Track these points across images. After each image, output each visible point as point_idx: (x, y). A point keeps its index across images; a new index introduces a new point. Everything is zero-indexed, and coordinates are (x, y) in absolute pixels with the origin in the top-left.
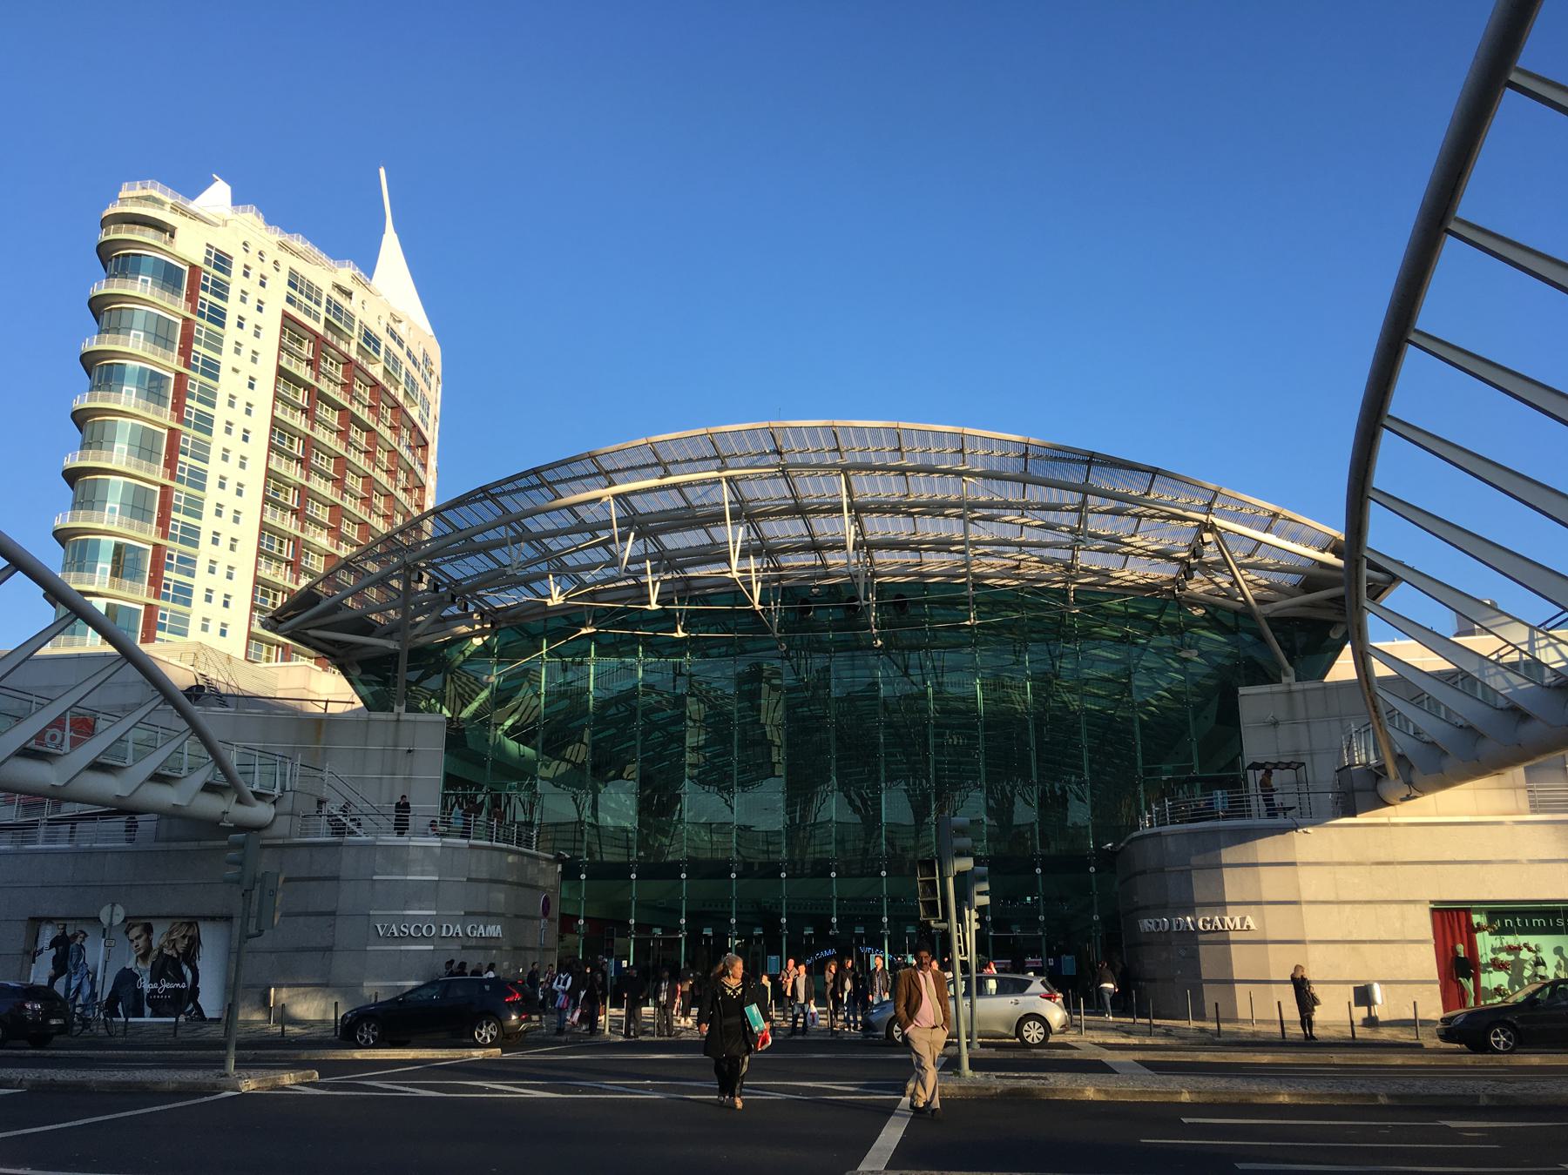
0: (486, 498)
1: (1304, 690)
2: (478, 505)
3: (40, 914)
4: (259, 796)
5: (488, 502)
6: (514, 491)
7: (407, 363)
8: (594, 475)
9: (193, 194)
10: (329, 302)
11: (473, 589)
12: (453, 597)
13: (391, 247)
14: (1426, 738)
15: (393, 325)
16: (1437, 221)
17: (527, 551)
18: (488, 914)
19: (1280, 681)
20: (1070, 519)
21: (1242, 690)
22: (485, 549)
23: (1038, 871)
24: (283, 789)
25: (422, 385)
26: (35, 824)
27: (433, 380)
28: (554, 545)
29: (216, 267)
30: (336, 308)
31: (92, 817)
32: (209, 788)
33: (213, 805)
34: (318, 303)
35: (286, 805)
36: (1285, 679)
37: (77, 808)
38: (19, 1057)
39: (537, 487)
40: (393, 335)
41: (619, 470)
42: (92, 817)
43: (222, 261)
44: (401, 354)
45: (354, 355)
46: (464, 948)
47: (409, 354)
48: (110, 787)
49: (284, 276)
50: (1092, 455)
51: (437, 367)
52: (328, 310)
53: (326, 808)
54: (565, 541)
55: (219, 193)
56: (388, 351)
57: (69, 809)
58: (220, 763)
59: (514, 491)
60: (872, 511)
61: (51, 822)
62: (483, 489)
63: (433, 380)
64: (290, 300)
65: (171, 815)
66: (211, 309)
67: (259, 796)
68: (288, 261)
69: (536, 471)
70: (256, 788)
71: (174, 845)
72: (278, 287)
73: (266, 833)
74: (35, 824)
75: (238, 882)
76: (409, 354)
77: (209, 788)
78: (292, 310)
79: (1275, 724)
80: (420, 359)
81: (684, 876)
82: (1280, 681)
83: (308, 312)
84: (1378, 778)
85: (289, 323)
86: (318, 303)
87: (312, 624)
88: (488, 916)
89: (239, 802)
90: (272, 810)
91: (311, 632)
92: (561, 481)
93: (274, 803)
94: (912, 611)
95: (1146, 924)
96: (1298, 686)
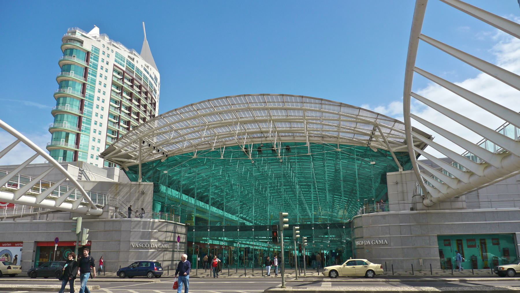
1: (405, 174)
7: (150, 79)
9: (88, 31)
10: (127, 61)
13: (146, 44)
15: (146, 67)
16: (415, 35)
19: (398, 171)
20: (336, 123)
21: (388, 174)
23: (344, 227)
25: (154, 85)
27: (158, 84)
28: (181, 132)
29: (95, 52)
34: (124, 61)
36: (400, 170)
37: (48, 210)
38: (212, 285)
40: (146, 70)
43: (97, 50)
44: (148, 76)
45: (134, 77)
47: (150, 76)
50: (341, 103)
51: (159, 80)
52: (127, 64)
55: (96, 31)
56: (144, 75)
60: (278, 122)
63: (158, 84)
64: (116, 61)
66: (93, 64)
67: (99, 207)
68: (115, 50)
72: (113, 56)
73: (100, 217)
74: (36, 214)
76: (150, 76)
79: (397, 183)
80: (154, 77)
81: (313, 228)
82: (398, 171)
83: (121, 64)
84: (423, 199)
85: (116, 68)
86: (124, 61)
90: (102, 210)
91: (113, 159)
93: (103, 208)
94: (292, 151)
95: (357, 243)
96: (404, 172)
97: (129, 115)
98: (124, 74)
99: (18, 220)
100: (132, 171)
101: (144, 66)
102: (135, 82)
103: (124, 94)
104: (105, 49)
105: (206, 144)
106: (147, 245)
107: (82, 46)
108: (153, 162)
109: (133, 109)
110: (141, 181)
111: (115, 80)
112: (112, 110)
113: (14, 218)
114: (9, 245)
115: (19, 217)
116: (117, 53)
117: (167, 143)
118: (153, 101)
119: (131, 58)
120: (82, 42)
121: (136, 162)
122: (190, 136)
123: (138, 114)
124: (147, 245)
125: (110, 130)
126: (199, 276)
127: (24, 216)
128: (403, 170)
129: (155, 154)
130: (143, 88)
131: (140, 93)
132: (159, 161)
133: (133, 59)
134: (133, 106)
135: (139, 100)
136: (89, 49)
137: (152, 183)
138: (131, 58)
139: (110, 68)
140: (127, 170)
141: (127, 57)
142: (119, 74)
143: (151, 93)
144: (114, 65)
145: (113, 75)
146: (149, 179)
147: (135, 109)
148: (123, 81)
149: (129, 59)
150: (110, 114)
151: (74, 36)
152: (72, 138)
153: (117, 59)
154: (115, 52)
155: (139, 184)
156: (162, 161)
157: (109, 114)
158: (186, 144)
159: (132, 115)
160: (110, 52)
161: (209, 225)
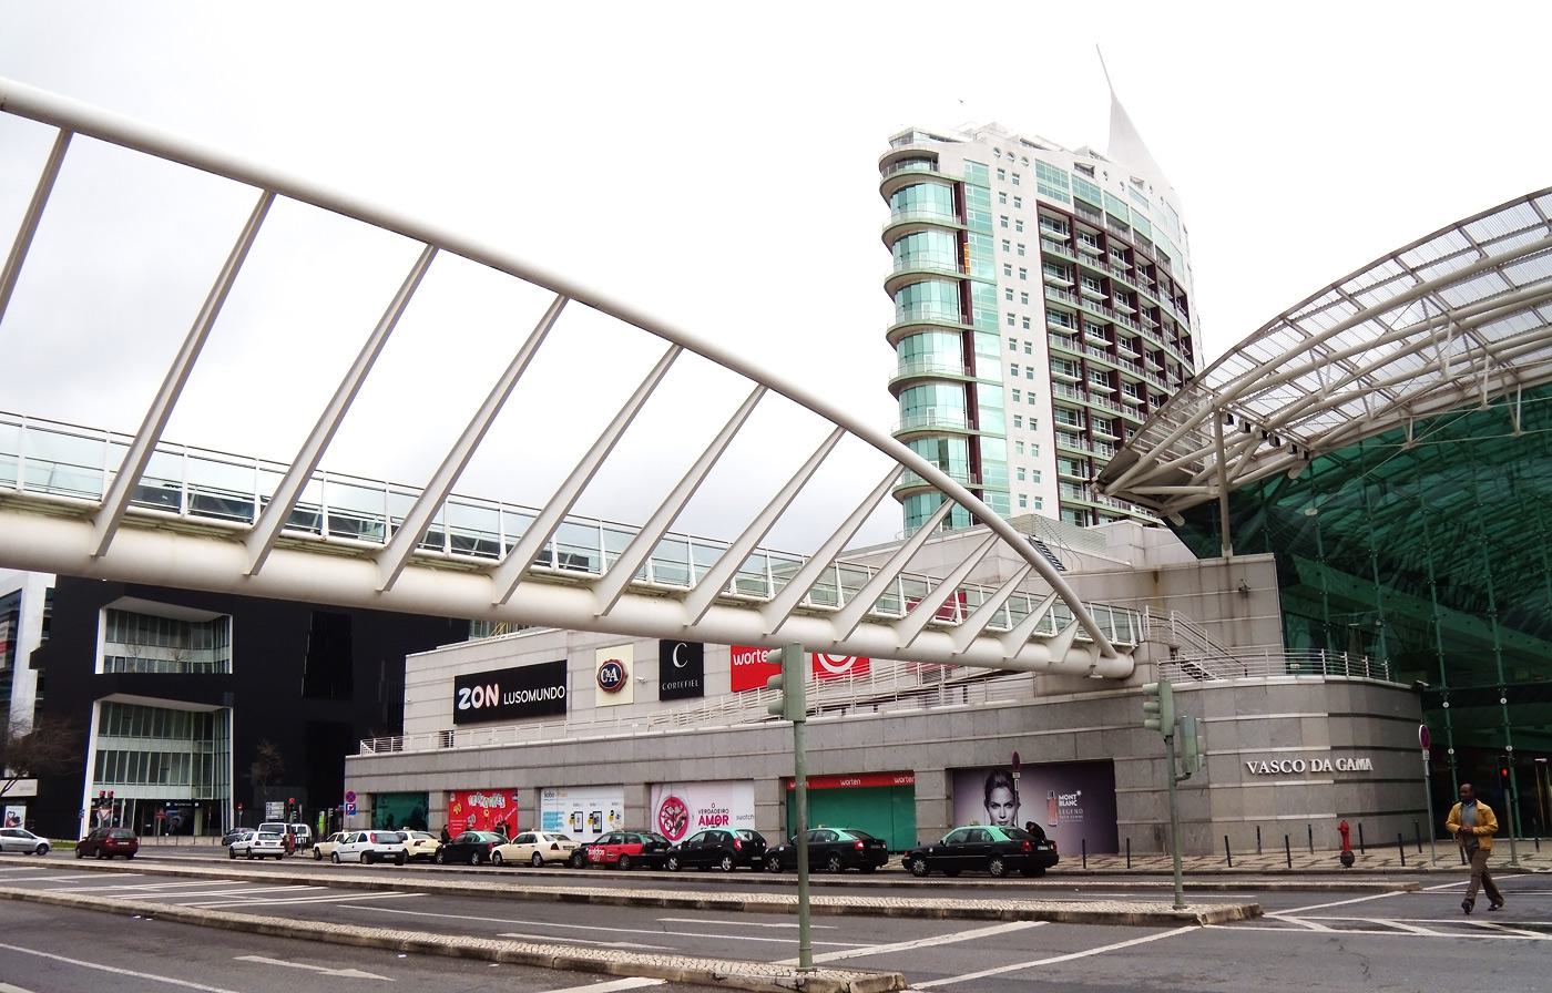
0: (1285, 325)
2: (1278, 334)
3: (541, 785)
4: (1119, 649)
5: (1288, 330)
6: (1313, 313)
8: (1399, 276)
11: (1282, 422)
12: (1264, 433)
14: (800, 761)
17: (1335, 373)
18: (1356, 748)
22: (1290, 379)
24: (1138, 641)
26: (936, 689)
30: (1081, 185)
31: (980, 679)
32: (1077, 645)
33: (1080, 660)
34: (1066, 185)
35: (1144, 654)
39: (1337, 302)
41: (1426, 265)
42: (980, 679)
45: (1106, 226)
46: (1336, 782)
48: (992, 650)
49: (1032, 169)
53: (1179, 656)
54: (1373, 356)
57: (958, 674)
58: (1085, 624)
59: (1313, 313)
61: (949, 686)
62: (1282, 317)
65: (1047, 671)
67: (1119, 649)
69: (1335, 286)
70: (1115, 641)
71: (1052, 700)
72: (1030, 177)
74: (936, 689)
75: (1159, 729)
77: (1077, 645)
78: (1045, 199)
82: (1221, 556)
83: (1058, 197)
85: (1046, 212)
86: (1066, 185)
87: (1135, 482)
88: (1358, 749)
89: (1103, 655)
92: (1363, 291)
93: (1132, 654)
97: (1111, 350)
98: (1071, 225)
99: (889, 710)
100: (1198, 526)
101: (1127, 183)
102: (1110, 241)
103: (1085, 289)
104: (1004, 162)
105: (1447, 391)
106: (1299, 764)
107: (936, 169)
108: (1262, 483)
109: (1118, 330)
110: (1231, 552)
111: (1050, 249)
112: (1057, 343)
113: (875, 703)
114: (386, 856)
115: (889, 699)
116: (1040, 165)
117: (1313, 406)
118: (1177, 292)
119: (1083, 169)
120: (932, 158)
121: (1212, 491)
122: (1392, 371)
123: (1136, 343)
124: (1299, 764)
125: (1063, 409)
126: (1523, 864)
127: (905, 695)
128: (1235, 554)
129: (1267, 454)
130: (1137, 257)
131: (1131, 273)
132: (1282, 473)
133: (1091, 172)
134: (1116, 321)
135: (1132, 298)
136: (957, 175)
137: (1270, 556)
138: (1083, 169)
139: (1030, 215)
140: (1180, 522)
141: (1070, 169)
142: (1057, 227)
143: (1165, 268)
144: (1040, 204)
145: (1042, 236)
146: (1253, 546)
147: (1125, 328)
148: (1073, 247)
149: (1079, 174)
150: (1053, 359)
151: (908, 147)
152: (957, 450)
153: (1045, 182)
154: (1032, 164)
155: (1228, 565)
156: (1292, 475)
157: (1052, 359)
158: (1379, 401)
159: (1121, 348)
160: (1018, 166)
161: (1502, 682)
